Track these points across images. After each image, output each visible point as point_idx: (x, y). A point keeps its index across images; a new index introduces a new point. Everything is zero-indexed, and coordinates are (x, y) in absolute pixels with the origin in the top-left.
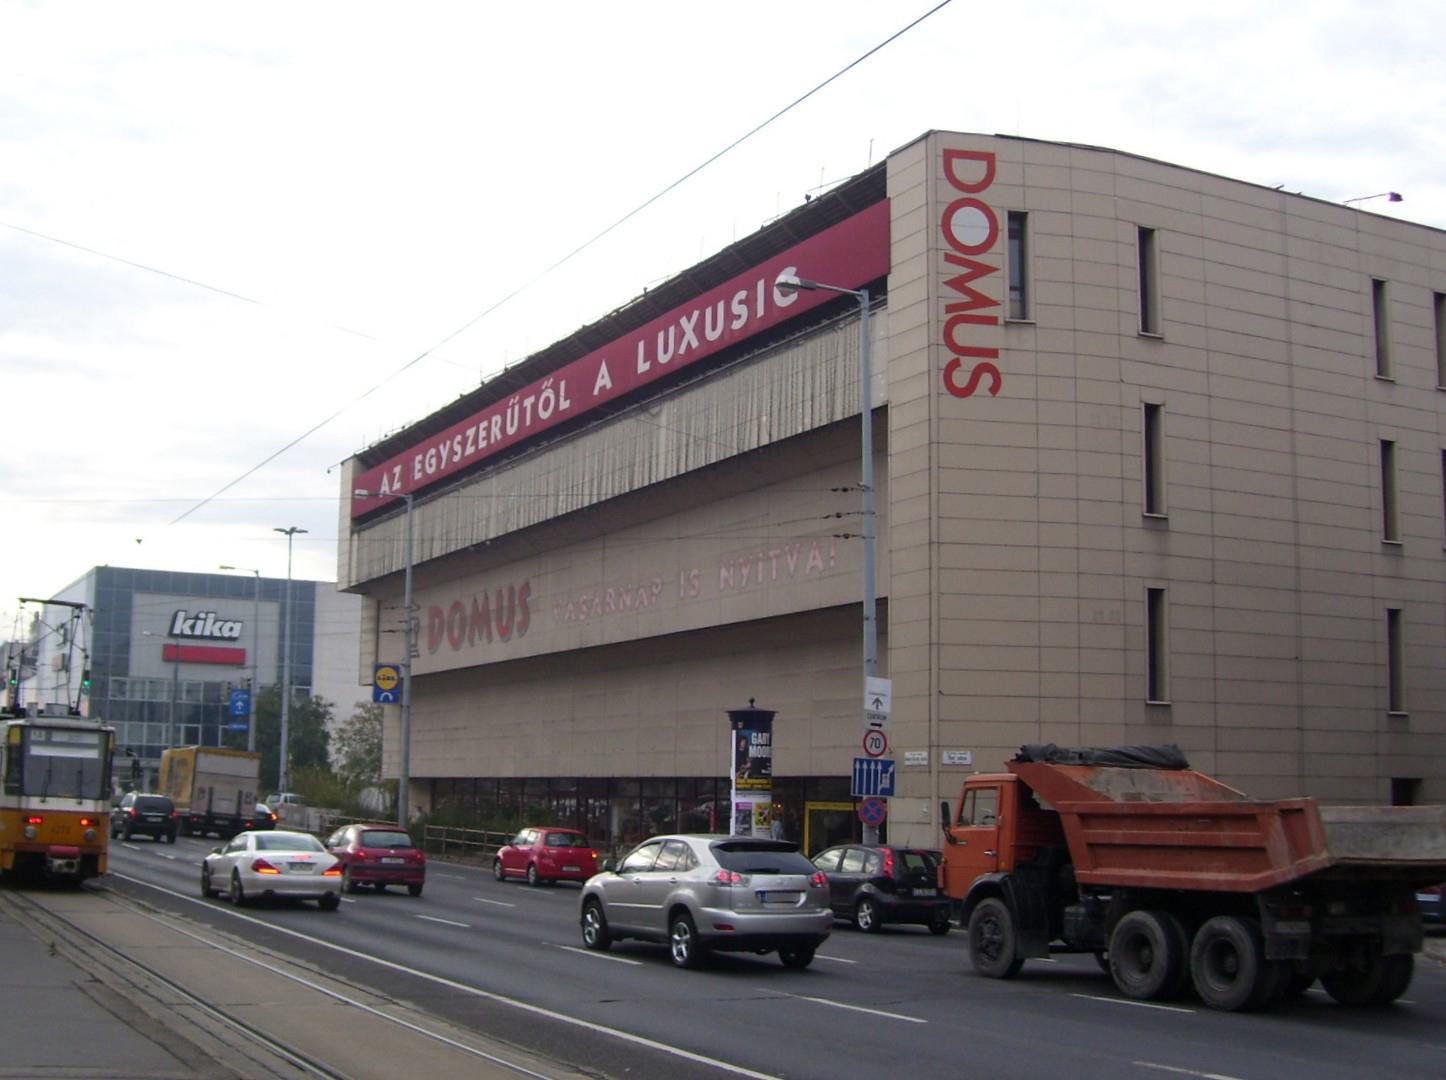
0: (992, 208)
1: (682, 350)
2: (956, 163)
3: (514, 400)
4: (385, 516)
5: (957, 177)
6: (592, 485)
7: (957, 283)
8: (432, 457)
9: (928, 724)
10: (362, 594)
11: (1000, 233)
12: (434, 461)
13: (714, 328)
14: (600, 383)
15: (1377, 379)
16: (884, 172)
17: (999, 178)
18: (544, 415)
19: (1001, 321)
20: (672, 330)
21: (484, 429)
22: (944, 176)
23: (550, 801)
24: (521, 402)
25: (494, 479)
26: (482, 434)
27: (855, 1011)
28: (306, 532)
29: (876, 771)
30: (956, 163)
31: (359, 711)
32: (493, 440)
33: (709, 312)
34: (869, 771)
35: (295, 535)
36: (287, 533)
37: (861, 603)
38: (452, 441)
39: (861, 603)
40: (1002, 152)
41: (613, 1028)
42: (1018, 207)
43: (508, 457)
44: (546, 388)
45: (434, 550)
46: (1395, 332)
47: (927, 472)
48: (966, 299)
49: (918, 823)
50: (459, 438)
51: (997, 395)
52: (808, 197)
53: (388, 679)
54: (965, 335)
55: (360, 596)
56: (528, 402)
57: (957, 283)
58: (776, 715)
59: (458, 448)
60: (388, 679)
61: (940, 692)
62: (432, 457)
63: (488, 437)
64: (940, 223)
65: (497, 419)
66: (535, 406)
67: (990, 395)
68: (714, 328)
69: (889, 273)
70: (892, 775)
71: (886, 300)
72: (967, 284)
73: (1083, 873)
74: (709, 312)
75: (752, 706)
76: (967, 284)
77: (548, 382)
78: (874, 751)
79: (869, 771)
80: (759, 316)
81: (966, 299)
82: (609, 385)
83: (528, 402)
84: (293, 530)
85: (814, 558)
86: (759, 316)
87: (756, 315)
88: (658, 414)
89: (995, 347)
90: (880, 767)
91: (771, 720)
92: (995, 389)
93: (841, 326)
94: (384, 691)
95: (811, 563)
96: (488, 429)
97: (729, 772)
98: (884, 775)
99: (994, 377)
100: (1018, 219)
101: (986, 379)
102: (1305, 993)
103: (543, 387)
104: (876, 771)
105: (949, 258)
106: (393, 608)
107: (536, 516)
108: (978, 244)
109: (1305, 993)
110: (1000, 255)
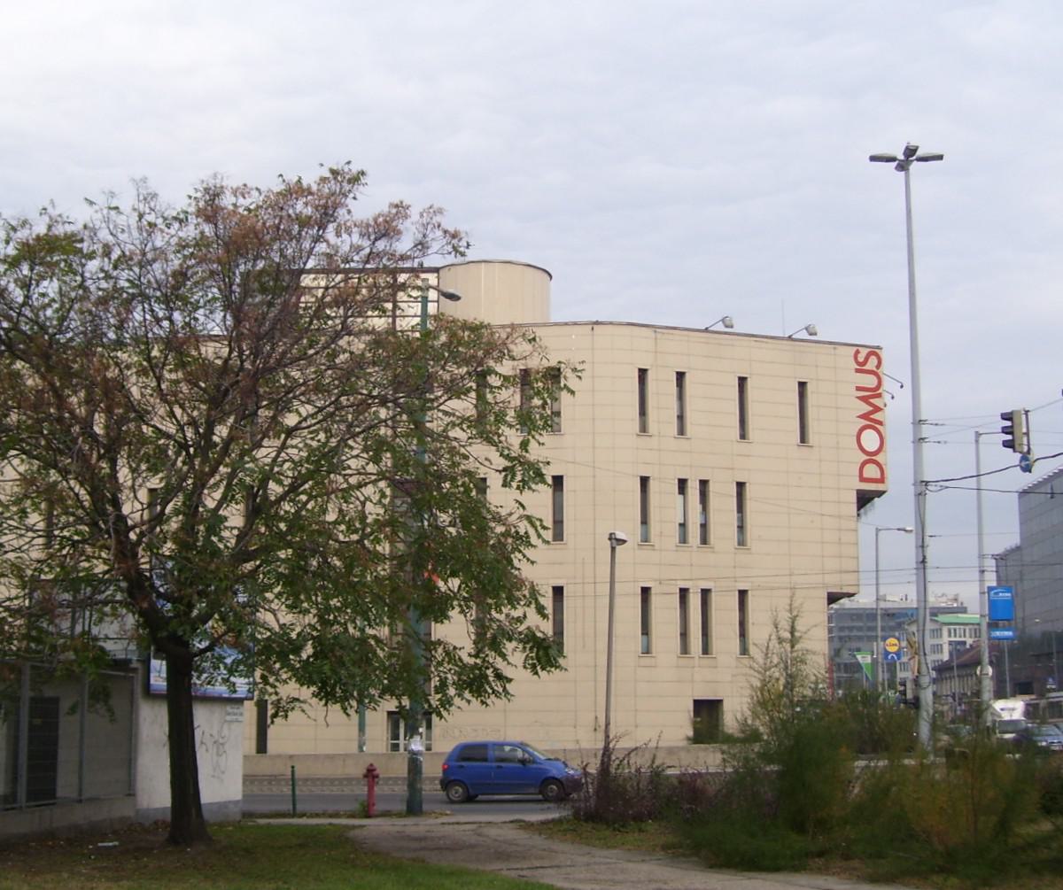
2: (878, 476)
5: (874, 465)
7: (877, 409)
9: (881, 581)
15: (706, 650)
30: (878, 476)
46: (619, 629)
47: (880, 568)
48: (872, 400)
53: (893, 645)
54: (870, 381)
57: (877, 409)
60: (893, 645)
72: (871, 409)
73: (135, 314)
76: (871, 409)
81: (872, 400)
94: (891, 653)
101: (861, 359)
102: (781, 767)
105: (881, 423)
109: (781, 767)
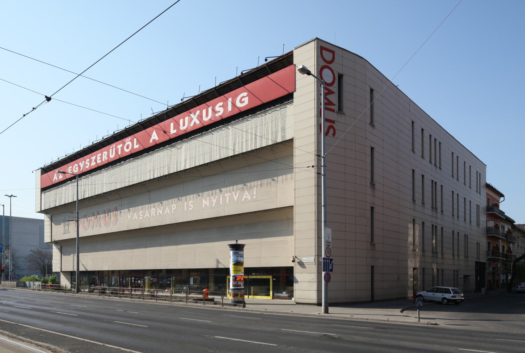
0: (334, 71)
1: (192, 125)
3: (114, 145)
4: (49, 190)
6: (89, 192)
8: (76, 167)
10: (45, 214)
11: (336, 80)
12: (77, 168)
13: (112, 154)
14: (54, 178)
16: (292, 55)
17: (335, 60)
18: (127, 150)
19: (336, 111)
20: (187, 118)
21: (99, 157)
22: (320, 56)
23: (126, 279)
24: (116, 147)
25: (105, 173)
26: (99, 158)
27: (251, 341)
28: (16, 197)
29: (328, 262)
31: (31, 253)
32: (103, 160)
33: (204, 111)
34: (327, 262)
35: (12, 197)
36: (9, 197)
37: (293, 206)
38: (85, 161)
39: (293, 206)
40: (337, 52)
41: (51, 331)
42: (341, 73)
43: (242, 117)
44: (128, 141)
45: (42, 208)
49: (309, 282)
50: (88, 160)
51: (334, 137)
52: (93, 143)
55: (44, 214)
56: (119, 147)
58: (245, 246)
59: (88, 164)
61: (319, 237)
62: (76, 167)
63: (102, 159)
64: (319, 73)
65: (106, 153)
66: (122, 148)
67: (332, 136)
68: (112, 154)
69: (295, 91)
70: (332, 264)
71: (293, 101)
74: (204, 111)
75: (237, 243)
77: (129, 138)
78: (328, 255)
79: (327, 262)
80: (229, 111)
82: (157, 138)
83: (119, 147)
84: (12, 196)
85: (246, 195)
86: (229, 111)
87: (228, 110)
88: (181, 148)
89: (334, 120)
90: (329, 261)
91: (244, 247)
92: (334, 134)
93: (269, 112)
95: (245, 197)
96: (101, 157)
97: (229, 265)
98: (330, 264)
99: (333, 129)
100: (341, 77)
101: (331, 131)
103: (126, 141)
104: (328, 262)
106: (72, 213)
107: (192, 165)
108: (332, 81)
110: (335, 88)
